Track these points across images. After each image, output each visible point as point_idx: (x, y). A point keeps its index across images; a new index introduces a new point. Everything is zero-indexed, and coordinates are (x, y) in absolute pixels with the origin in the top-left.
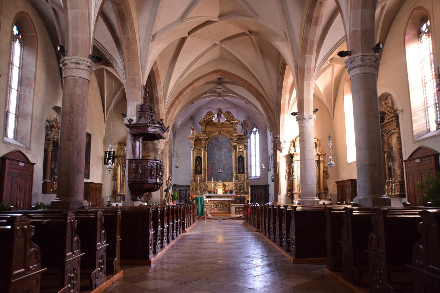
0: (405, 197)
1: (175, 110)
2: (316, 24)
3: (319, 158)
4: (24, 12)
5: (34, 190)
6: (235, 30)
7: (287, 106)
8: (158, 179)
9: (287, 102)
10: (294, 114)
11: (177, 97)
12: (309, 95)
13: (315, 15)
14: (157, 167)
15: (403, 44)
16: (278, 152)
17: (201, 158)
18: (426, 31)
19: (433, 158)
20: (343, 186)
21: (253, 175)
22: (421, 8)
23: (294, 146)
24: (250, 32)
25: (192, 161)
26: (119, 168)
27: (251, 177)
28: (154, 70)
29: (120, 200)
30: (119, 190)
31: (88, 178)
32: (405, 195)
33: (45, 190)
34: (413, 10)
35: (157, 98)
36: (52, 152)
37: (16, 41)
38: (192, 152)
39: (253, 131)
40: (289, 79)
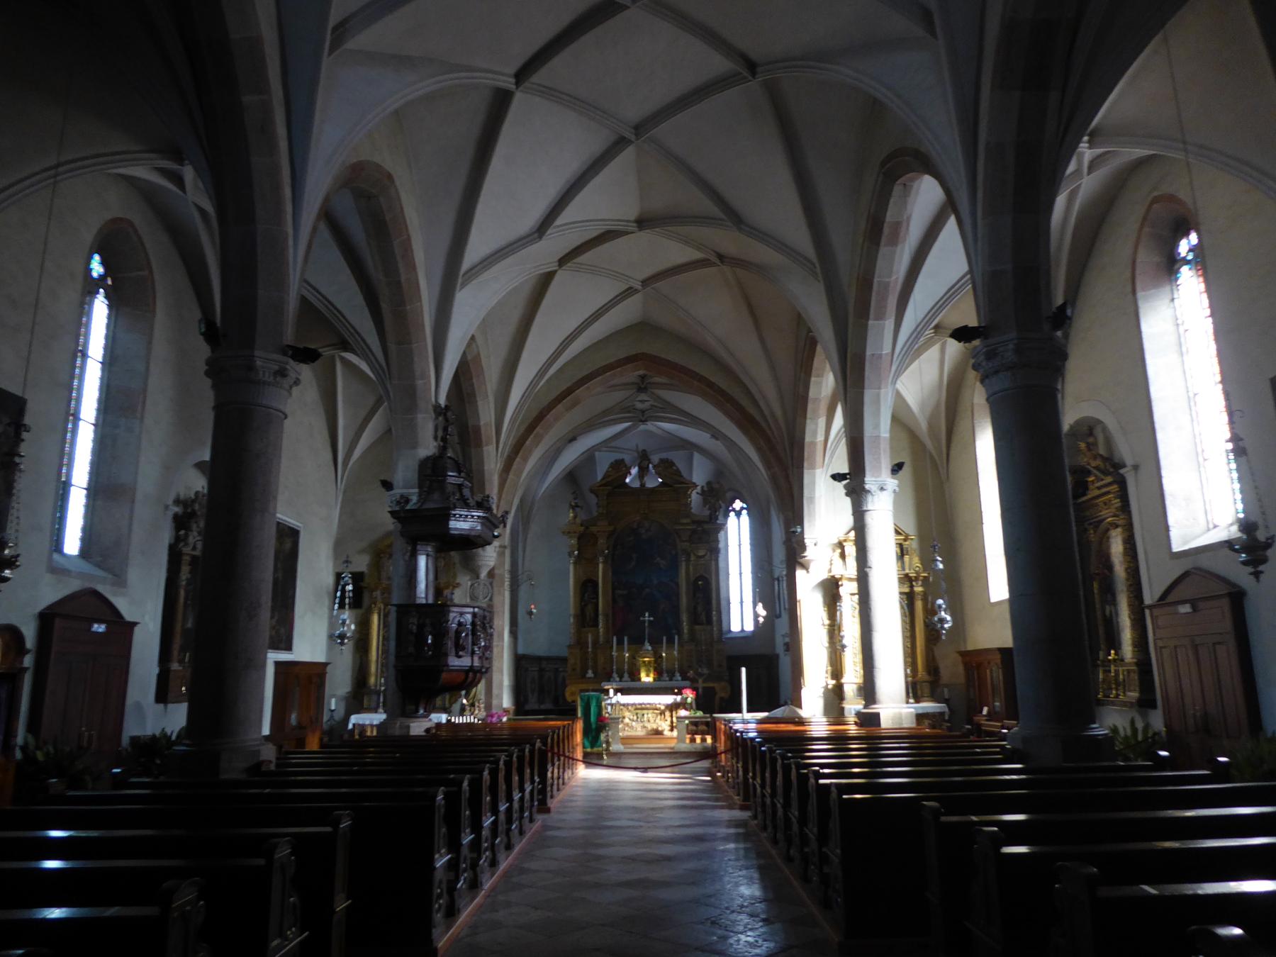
0: (1154, 706)
1: (525, 460)
2: (895, 240)
3: (912, 587)
4: (121, 219)
5: (133, 695)
6: (678, 253)
7: (820, 448)
8: (476, 658)
9: (820, 438)
10: (837, 477)
11: (531, 429)
12: (877, 426)
13: (890, 217)
14: (473, 624)
15: (1129, 289)
16: (800, 574)
17: (596, 584)
18: (1190, 257)
19: (1225, 603)
20: (979, 666)
21: (735, 627)
22: (1171, 198)
23: (843, 556)
24: (721, 257)
25: (572, 593)
26: (375, 618)
27: (730, 631)
28: (469, 358)
29: (373, 705)
30: (372, 680)
31: (288, 647)
32: (1154, 701)
33: (163, 696)
34: (1152, 203)
35: (477, 430)
36: (188, 584)
37: (98, 293)
38: (571, 568)
39: (734, 510)
40: (825, 383)
